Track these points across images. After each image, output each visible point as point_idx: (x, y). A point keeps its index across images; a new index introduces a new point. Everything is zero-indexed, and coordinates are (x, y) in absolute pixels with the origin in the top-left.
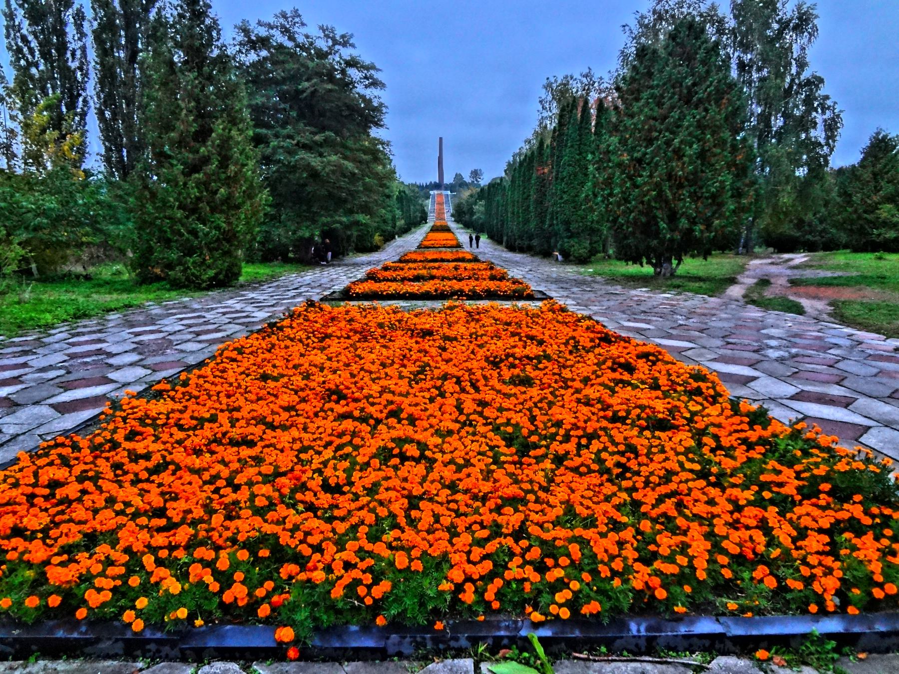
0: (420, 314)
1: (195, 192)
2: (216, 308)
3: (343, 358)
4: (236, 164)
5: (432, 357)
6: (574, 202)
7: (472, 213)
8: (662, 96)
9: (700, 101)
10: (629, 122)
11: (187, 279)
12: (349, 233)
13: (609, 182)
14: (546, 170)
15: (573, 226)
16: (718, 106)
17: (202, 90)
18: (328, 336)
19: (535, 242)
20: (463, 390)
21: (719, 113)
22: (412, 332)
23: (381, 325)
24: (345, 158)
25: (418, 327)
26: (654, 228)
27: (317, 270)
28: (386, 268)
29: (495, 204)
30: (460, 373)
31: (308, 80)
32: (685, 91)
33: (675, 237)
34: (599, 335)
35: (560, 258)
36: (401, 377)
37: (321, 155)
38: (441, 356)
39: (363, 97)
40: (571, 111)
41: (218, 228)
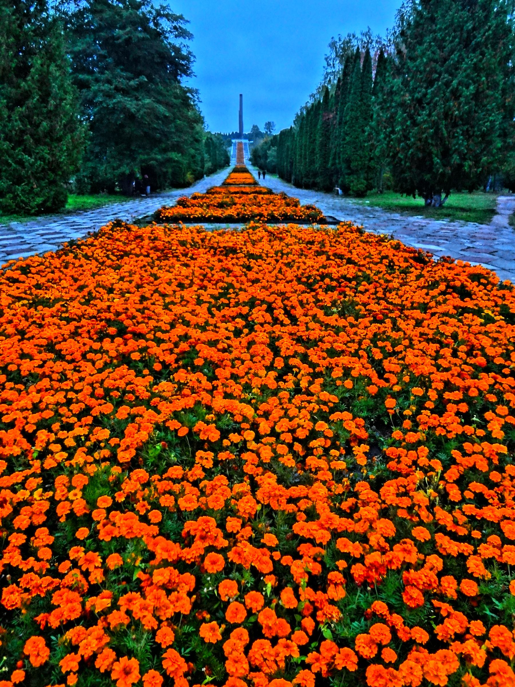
0: (224, 233)
1: (18, 125)
2: (37, 230)
3: (136, 278)
4: (55, 99)
5: (235, 276)
6: (354, 142)
7: (266, 157)
8: (443, 40)
9: (478, 45)
10: (410, 64)
11: (17, 205)
12: (164, 170)
13: (391, 121)
14: (331, 116)
15: (353, 164)
16: (495, 50)
17: (21, 26)
18: (127, 254)
19: (318, 180)
20: (276, 321)
21: (494, 56)
22: (214, 250)
23: (183, 243)
24: (159, 102)
25: (222, 245)
26: (428, 163)
27: (137, 201)
28: (194, 198)
29: (285, 149)
30: (272, 298)
31: (123, 28)
32: (465, 35)
33: (446, 171)
34: (412, 255)
35: (340, 192)
36: (199, 302)
37: (137, 99)
38: (246, 275)
39: (174, 47)
40: (355, 61)
41: (42, 159)
